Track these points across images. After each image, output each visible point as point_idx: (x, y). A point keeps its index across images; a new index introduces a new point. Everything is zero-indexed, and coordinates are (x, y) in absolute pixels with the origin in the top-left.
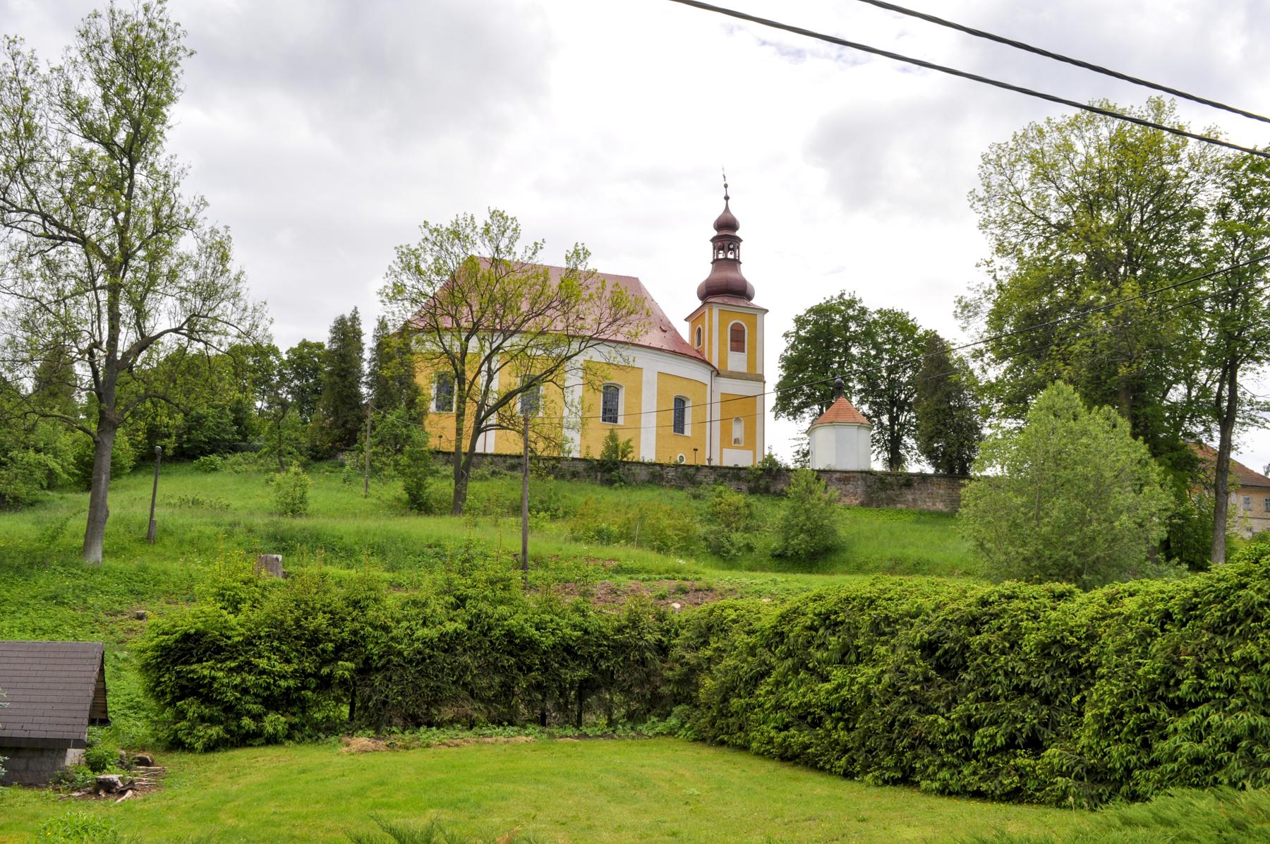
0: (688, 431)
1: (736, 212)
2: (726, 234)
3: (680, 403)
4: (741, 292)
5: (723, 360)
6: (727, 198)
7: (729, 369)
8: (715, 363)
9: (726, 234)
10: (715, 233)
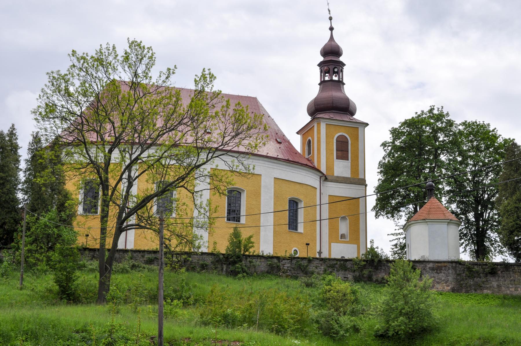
0: (301, 228)
1: (339, 41)
2: (331, 59)
3: (294, 204)
4: (345, 108)
5: (330, 167)
6: (331, 29)
7: (335, 175)
8: (323, 169)
9: (331, 59)
10: (322, 59)
